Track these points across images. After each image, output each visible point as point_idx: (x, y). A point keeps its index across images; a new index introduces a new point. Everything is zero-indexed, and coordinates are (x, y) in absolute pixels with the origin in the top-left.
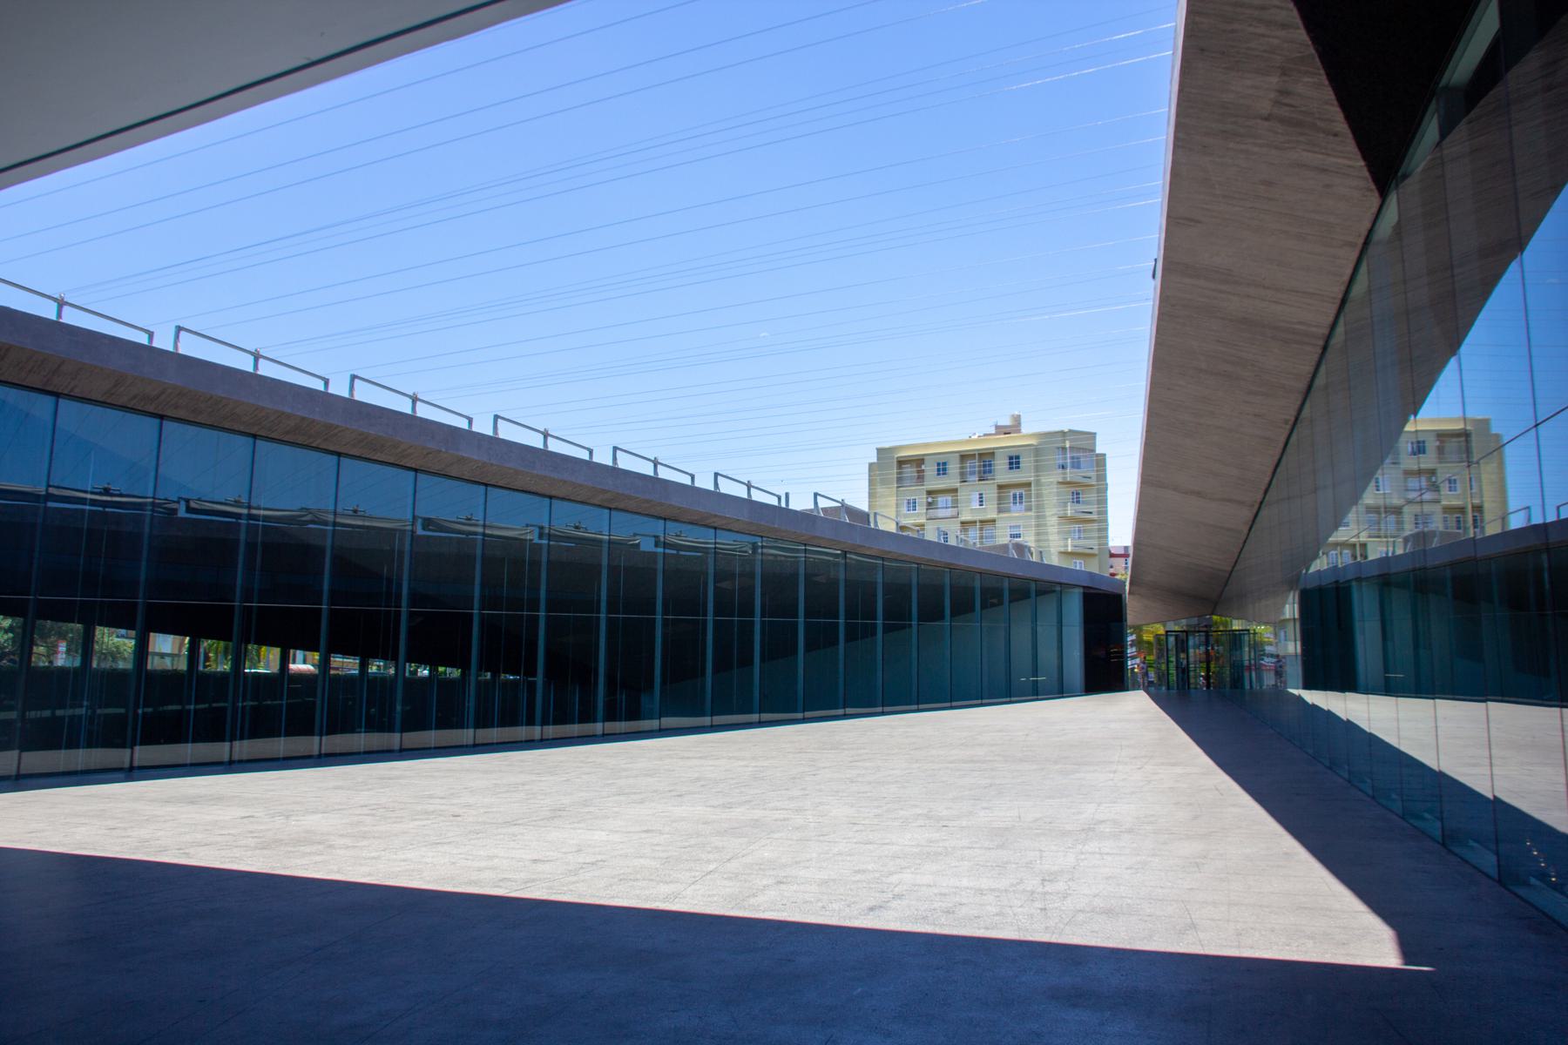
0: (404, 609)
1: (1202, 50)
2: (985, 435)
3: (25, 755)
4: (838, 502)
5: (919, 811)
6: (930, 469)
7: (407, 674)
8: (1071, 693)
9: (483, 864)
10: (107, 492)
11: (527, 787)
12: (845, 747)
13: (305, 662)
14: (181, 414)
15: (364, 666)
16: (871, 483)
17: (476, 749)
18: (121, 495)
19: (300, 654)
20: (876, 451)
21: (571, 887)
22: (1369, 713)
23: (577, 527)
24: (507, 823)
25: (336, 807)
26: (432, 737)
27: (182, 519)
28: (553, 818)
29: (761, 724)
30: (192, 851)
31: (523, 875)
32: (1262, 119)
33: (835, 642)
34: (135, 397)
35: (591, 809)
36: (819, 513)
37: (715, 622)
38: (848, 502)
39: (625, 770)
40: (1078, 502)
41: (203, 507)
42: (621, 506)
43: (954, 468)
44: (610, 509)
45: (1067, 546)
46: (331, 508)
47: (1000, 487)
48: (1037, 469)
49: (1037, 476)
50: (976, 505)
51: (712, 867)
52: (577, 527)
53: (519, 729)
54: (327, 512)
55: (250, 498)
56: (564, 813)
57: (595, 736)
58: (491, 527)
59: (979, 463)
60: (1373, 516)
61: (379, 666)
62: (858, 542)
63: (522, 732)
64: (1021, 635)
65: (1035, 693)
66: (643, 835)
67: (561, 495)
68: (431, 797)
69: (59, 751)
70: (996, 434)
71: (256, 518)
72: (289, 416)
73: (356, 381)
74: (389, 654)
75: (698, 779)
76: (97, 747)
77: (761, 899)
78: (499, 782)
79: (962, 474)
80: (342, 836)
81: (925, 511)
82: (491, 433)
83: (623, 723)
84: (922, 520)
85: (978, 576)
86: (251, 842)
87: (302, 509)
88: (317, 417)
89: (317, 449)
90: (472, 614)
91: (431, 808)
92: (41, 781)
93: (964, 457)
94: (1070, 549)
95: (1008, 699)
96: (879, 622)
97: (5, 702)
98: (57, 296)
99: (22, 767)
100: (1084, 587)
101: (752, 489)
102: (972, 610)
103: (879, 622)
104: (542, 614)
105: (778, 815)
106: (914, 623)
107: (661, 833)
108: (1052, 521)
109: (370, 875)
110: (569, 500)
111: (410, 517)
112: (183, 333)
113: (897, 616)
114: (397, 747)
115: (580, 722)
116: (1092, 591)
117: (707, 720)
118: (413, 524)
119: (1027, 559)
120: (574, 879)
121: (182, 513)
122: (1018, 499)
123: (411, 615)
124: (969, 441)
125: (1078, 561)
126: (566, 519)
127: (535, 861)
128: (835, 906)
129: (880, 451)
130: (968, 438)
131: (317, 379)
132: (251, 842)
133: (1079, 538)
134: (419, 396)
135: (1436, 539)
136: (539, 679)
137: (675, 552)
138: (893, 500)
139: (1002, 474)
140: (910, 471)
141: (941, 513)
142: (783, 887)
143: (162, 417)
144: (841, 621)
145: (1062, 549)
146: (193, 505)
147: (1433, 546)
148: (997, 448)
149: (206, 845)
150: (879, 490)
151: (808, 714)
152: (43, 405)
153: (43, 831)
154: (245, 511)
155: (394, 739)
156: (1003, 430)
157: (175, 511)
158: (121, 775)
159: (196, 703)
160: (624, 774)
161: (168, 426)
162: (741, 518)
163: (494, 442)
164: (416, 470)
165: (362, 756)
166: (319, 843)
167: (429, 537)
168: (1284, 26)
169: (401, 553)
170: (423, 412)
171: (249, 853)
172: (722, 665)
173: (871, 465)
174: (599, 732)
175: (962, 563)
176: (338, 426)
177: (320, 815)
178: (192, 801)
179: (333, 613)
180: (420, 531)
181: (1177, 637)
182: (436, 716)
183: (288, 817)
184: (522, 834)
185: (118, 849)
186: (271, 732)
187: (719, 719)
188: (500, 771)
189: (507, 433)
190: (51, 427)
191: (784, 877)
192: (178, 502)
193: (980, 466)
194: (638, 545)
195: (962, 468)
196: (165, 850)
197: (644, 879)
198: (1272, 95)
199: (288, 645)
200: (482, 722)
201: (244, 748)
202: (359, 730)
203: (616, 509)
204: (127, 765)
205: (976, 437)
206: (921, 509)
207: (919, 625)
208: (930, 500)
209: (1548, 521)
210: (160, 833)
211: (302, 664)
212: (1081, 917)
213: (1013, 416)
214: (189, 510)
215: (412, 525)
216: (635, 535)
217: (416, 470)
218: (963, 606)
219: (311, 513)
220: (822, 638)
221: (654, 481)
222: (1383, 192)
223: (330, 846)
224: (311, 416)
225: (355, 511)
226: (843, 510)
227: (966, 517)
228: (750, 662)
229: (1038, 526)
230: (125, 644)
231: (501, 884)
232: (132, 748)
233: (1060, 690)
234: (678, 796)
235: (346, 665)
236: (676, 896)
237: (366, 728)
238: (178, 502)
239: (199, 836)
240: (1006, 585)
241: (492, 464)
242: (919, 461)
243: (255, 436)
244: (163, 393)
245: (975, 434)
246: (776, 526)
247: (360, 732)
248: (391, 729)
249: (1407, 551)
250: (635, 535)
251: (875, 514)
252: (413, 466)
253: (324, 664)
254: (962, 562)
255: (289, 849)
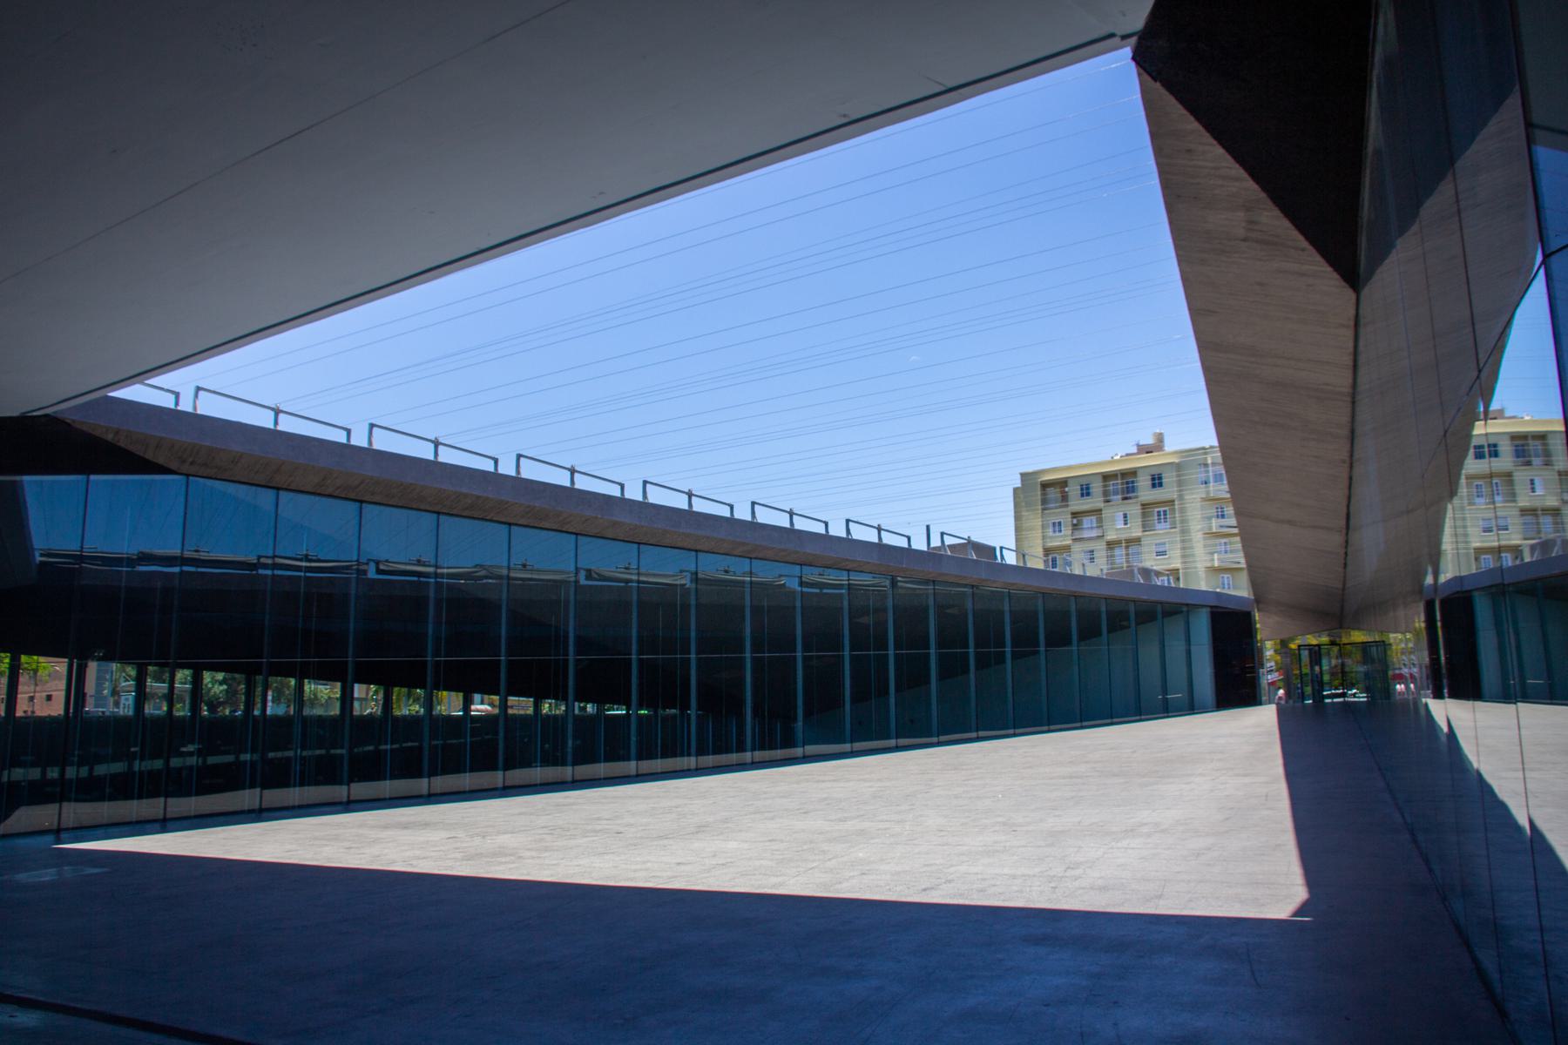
0: (571, 658)
1: (1179, 196)
2: (1127, 455)
3: (266, 792)
4: (963, 538)
5: (1000, 819)
6: (1073, 490)
7: (577, 712)
8: (1203, 709)
9: (638, 867)
10: (307, 558)
11: (679, 809)
12: (964, 767)
13: (482, 703)
14: (376, 498)
15: (537, 706)
16: (1016, 505)
17: (640, 778)
18: (319, 561)
19: (477, 697)
20: (1019, 476)
21: (703, 881)
22: (1475, 722)
23: (726, 572)
24: (660, 838)
25: (522, 829)
26: (601, 769)
27: (374, 580)
28: (697, 832)
29: (898, 749)
30: (414, 862)
31: (669, 874)
32: (1242, 240)
33: (966, 671)
34: (338, 488)
35: (729, 825)
36: (945, 550)
37: (852, 657)
38: (974, 539)
39: (765, 793)
40: (1223, 516)
41: (391, 569)
42: (760, 555)
43: (1097, 487)
44: (751, 558)
45: (1213, 560)
46: (505, 564)
47: (1144, 506)
48: (1180, 483)
49: (1180, 491)
50: (1120, 525)
51: (815, 864)
52: (726, 572)
53: (730, 756)
54: (501, 567)
55: (437, 556)
56: (708, 829)
57: (745, 764)
58: (647, 575)
59: (1122, 482)
60: (1529, 519)
61: (550, 704)
62: (983, 577)
63: (734, 757)
64: (1149, 655)
65: (1166, 710)
66: (767, 844)
67: (706, 549)
68: (599, 819)
69: (286, 789)
70: (1138, 453)
71: (442, 576)
72: (466, 495)
73: (522, 459)
74: (559, 694)
75: (825, 799)
76: (309, 785)
77: (845, 885)
78: (656, 805)
79: (1106, 493)
80: (529, 850)
81: (1070, 532)
82: (640, 498)
83: (779, 751)
84: (1068, 542)
85: (1073, 599)
86: (459, 856)
87: (476, 566)
88: (491, 496)
89: (491, 521)
90: (631, 659)
91: (599, 827)
92: (370, 805)
93: (1106, 477)
94: (1216, 564)
95: (1138, 718)
96: (1008, 649)
97: (223, 748)
98: (273, 406)
99: (263, 804)
100: (1211, 607)
101: (882, 532)
102: (1100, 634)
103: (1008, 649)
104: (693, 656)
105: (881, 826)
106: (1042, 649)
107: (782, 841)
108: (1197, 537)
109: (552, 876)
110: (713, 553)
111: (572, 568)
112: (375, 429)
113: (1025, 641)
114: (570, 779)
115: (737, 752)
116: (1219, 610)
117: (847, 747)
118: (577, 574)
119: (1153, 583)
120: (708, 875)
121: (372, 574)
122: (1162, 517)
123: (577, 662)
124: (1113, 462)
125: (1226, 576)
126: (712, 566)
127: (679, 864)
128: (898, 889)
129: (1023, 475)
130: (1110, 459)
131: (488, 460)
132: (459, 856)
133: (1226, 552)
134: (577, 468)
135: (1556, 549)
136: (692, 712)
137: (817, 591)
138: (1038, 522)
139: (1146, 493)
140: (1053, 493)
141: (1086, 534)
142: (864, 876)
143: (361, 502)
144: (971, 650)
145: (1209, 565)
146: (382, 567)
147: (1553, 555)
148: (1139, 468)
149: (424, 858)
150: (1023, 513)
151: (942, 738)
152: (265, 498)
153: (297, 850)
154: (431, 570)
155: (567, 772)
156: (1146, 450)
157: (365, 572)
158: (340, 808)
159: (392, 744)
160: (764, 796)
161: (367, 508)
162: (870, 561)
163: (644, 507)
164: (577, 534)
165: (539, 787)
166: (511, 855)
167: (590, 586)
168: (1237, 179)
169: (567, 602)
170: (582, 483)
171: (458, 863)
172: (860, 697)
173: (1015, 490)
174: (693, 765)
175: (1086, 591)
176: (508, 502)
177: (510, 835)
178: (405, 826)
179: (510, 663)
180: (583, 581)
181: (1310, 650)
182: (605, 751)
183: (484, 837)
184: (671, 845)
185: (358, 862)
186: (457, 769)
187: (858, 746)
188: (659, 797)
189: (531, 472)
190: (273, 515)
191: (868, 870)
192: (367, 564)
193: (1122, 484)
194: (784, 584)
195: (1105, 486)
196: (394, 862)
197: (760, 874)
198: (1244, 224)
199: (468, 686)
200: (645, 753)
201: (441, 782)
202: (534, 765)
203: (756, 558)
204: (345, 799)
205: (1118, 457)
206: (1067, 531)
207: (1046, 651)
208: (1075, 521)
209: (1463, 574)
210: (386, 851)
211: (481, 707)
212: (1080, 892)
213: (1155, 433)
214: (379, 571)
215: (576, 576)
216: (781, 576)
217: (577, 534)
218: (1090, 631)
219: (485, 569)
220: (953, 668)
221: (791, 532)
222: (1353, 276)
223: (520, 857)
224: (485, 495)
225: (524, 566)
226: (970, 546)
227: (1111, 536)
228: (887, 693)
229: (1183, 541)
230: (321, 691)
231: (651, 879)
232: (348, 785)
233: (1191, 707)
234: (805, 813)
235: (521, 705)
236: (781, 884)
237: (541, 762)
238: (367, 564)
239: (418, 853)
240: (1132, 608)
241: (642, 527)
242: (1063, 483)
243: (438, 513)
244: (362, 482)
245: (1116, 455)
246: (904, 566)
247: (537, 767)
248: (564, 764)
249: (1534, 559)
250: (781, 576)
251: (1001, 548)
252: (574, 531)
253: (504, 706)
254: (1087, 590)
255: (489, 859)
